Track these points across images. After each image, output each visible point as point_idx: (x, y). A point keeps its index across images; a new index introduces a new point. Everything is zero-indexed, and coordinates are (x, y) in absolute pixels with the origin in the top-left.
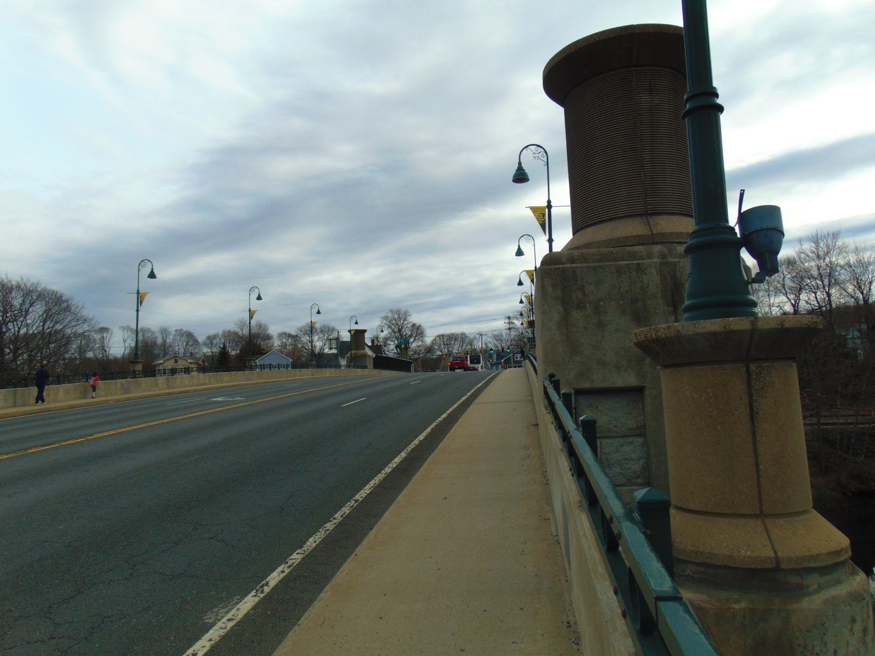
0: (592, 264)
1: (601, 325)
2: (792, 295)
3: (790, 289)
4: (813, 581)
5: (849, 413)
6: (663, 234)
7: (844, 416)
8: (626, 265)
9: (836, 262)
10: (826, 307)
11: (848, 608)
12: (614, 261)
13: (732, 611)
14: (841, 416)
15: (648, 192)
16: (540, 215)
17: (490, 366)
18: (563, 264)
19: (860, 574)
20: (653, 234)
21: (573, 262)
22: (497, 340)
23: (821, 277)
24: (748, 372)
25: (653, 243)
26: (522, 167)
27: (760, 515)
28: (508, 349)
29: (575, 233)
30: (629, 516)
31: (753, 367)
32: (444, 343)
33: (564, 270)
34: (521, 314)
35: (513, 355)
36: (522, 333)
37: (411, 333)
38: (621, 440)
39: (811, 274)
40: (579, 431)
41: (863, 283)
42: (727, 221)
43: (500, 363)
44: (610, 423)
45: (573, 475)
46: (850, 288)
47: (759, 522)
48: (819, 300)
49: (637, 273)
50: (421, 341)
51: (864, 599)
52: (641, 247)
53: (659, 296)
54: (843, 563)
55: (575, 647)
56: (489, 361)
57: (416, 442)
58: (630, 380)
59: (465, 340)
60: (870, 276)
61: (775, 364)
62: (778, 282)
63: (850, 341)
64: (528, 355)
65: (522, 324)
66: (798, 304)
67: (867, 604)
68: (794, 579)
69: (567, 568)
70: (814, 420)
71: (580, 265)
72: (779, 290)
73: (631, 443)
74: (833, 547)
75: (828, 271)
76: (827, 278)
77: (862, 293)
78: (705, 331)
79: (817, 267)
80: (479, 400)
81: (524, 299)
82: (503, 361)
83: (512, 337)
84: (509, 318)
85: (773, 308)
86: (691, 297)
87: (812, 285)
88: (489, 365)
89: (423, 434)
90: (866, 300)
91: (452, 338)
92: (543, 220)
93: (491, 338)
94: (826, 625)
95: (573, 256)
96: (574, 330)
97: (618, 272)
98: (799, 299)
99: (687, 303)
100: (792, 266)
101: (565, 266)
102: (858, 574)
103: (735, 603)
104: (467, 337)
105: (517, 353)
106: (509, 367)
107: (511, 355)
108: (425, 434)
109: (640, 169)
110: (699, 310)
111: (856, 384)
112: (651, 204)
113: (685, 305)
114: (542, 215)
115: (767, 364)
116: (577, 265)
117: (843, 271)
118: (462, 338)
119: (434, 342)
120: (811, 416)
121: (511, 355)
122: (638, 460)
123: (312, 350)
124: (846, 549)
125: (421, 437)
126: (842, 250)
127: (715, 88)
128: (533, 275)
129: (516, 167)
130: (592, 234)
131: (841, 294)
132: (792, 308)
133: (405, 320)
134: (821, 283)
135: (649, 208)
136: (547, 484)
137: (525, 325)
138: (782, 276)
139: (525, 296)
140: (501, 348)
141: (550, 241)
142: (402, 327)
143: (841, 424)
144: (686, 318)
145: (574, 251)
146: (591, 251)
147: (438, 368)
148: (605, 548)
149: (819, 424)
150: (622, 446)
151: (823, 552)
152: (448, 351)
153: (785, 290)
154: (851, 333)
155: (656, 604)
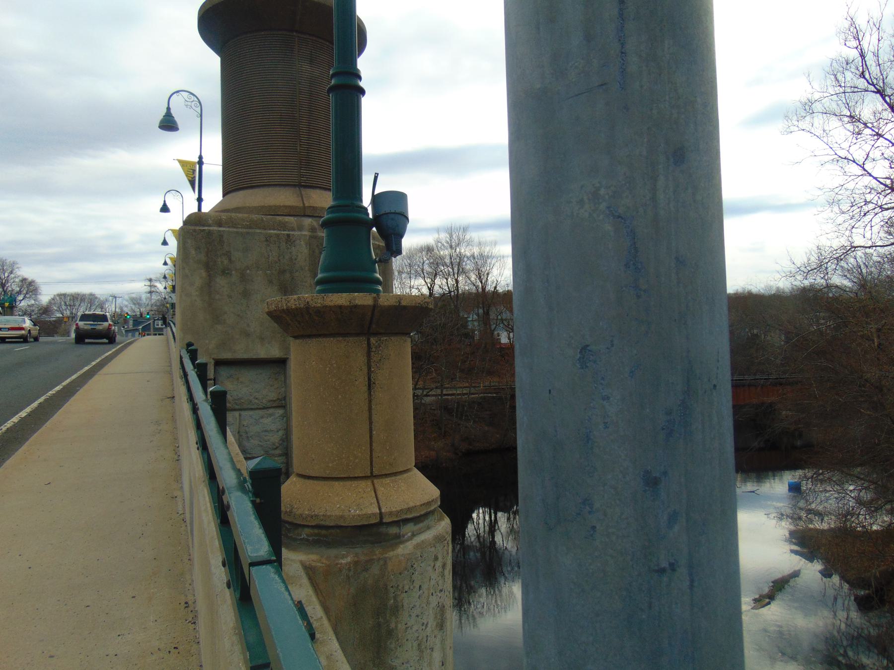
0: (240, 230)
1: (246, 294)
2: (429, 279)
3: (427, 274)
4: (408, 529)
5: (465, 385)
6: (314, 208)
7: (461, 387)
8: (276, 234)
9: (464, 254)
10: (454, 292)
11: (433, 549)
12: (263, 229)
13: (339, 566)
14: (459, 388)
15: (302, 163)
16: (190, 170)
17: (124, 333)
18: (210, 226)
19: (445, 519)
20: (304, 207)
21: (220, 224)
22: (134, 304)
23: (452, 266)
24: (369, 344)
25: (304, 216)
26: (171, 114)
27: (372, 476)
28: (148, 314)
29: (225, 194)
30: (241, 486)
31: (373, 340)
32: (65, 303)
33: (210, 233)
34: (165, 277)
35: (154, 322)
36: (165, 298)
37: (20, 290)
38: (261, 412)
39: (445, 262)
40: (208, 403)
41: (483, 273)
42: (361, 201)
43: (137, 330)
44: (251, 395)
45: (198, 449)
46: (473, 277)
47: (369, 483)
48: (449, 286)
49: (286, 243)
50: (35, 300)
51: (446, 540)
52: (292, 218)
53: (307, 268)
54: (432, 512)
55: (192, 626)
56: (124, 327)
57: (15, 419)
58: (275, 352)
59: (94, 302)
60: (488, 268)
61: (392, 338)
62: (419, 266)
63: (470, 323)
64: (170, 322)
65: (165, 288)
66: (433, 287)
67: (448, 544)
68: (393, 530)
69: (191, 545)
70: (439, 391)
71: (228, 229)
72: (419, 273)
73: (271, 415)
74: (426, 499)
75: (458, 261)
76: (457, 266)
77: (481, 282)
78: (332, 304)
79: (449, 256)
80: (106, 370)
81: (169, 261)
82: (141, 327)
83: (153, 301)
84: (150, 280)
85: (413, 290)
86: (323, 271)
87: (445, 272)
88: (124, 331)
89: (26, 409)
90: (484, 289)
91: (77, 298)
92: (192, 176)
93: (127, 301)
94: (415, 566)
95: (221, 220)
96: (217, 297)
97: (267, 240)
98: (435, 284)
99: (320, 276)
100: (431, 253)
101: (211, 228)
102: (444, 520)
103: (342, 558)
104: (96, 298)
105: (158, 319)
106: (148, 335)
107: (151, 322)
108: (28, 410)
109: (296, 139)
110: (330, 284)
111: (472, 361)
112: (305, 176)
113: (317, 277)
114: (192, 171)
115: (385, 338)
116: (224, 229)
117: (468, 262)
118: (91, 299)
119: (53, 302)
120: (437, 388)
121: (151, 322)
122: (278, 431)
124: (436, 499)
125: (23, 414)
126: (469, 243)
127: (358, 70)
129: (165, 111)
130: (243, 198)
131: (466, 282)
132: (428, 291)
133: (11, 272)
134: (452, 270)
135: (302, 180)
136: (178, 460)
137: (168, 290)
138: (422, 261)
139: (170, 258)
140: (139, 313)
141: (200, 200)
142: (7, 281)
143: (458, 395)
144: (319, 290)
145: (223, 214)
146: (240, 215)
147: (57, 333)
148: (219, 521)
149: (442, 395)
150: (262, 417)
151: (418, 504)
152: (72, 313)
153: (424, 274)
154: (471, 316)
155: (249, 569)
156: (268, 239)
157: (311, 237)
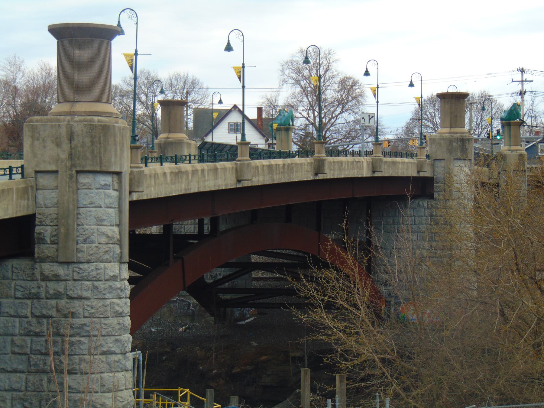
1: (44, 147)
18: (33, 122)
38: (51, 191)
73: (55, 192)
123: (153, 125)
128: (240, 72)
156: (52, 126)
157: (68, 124)
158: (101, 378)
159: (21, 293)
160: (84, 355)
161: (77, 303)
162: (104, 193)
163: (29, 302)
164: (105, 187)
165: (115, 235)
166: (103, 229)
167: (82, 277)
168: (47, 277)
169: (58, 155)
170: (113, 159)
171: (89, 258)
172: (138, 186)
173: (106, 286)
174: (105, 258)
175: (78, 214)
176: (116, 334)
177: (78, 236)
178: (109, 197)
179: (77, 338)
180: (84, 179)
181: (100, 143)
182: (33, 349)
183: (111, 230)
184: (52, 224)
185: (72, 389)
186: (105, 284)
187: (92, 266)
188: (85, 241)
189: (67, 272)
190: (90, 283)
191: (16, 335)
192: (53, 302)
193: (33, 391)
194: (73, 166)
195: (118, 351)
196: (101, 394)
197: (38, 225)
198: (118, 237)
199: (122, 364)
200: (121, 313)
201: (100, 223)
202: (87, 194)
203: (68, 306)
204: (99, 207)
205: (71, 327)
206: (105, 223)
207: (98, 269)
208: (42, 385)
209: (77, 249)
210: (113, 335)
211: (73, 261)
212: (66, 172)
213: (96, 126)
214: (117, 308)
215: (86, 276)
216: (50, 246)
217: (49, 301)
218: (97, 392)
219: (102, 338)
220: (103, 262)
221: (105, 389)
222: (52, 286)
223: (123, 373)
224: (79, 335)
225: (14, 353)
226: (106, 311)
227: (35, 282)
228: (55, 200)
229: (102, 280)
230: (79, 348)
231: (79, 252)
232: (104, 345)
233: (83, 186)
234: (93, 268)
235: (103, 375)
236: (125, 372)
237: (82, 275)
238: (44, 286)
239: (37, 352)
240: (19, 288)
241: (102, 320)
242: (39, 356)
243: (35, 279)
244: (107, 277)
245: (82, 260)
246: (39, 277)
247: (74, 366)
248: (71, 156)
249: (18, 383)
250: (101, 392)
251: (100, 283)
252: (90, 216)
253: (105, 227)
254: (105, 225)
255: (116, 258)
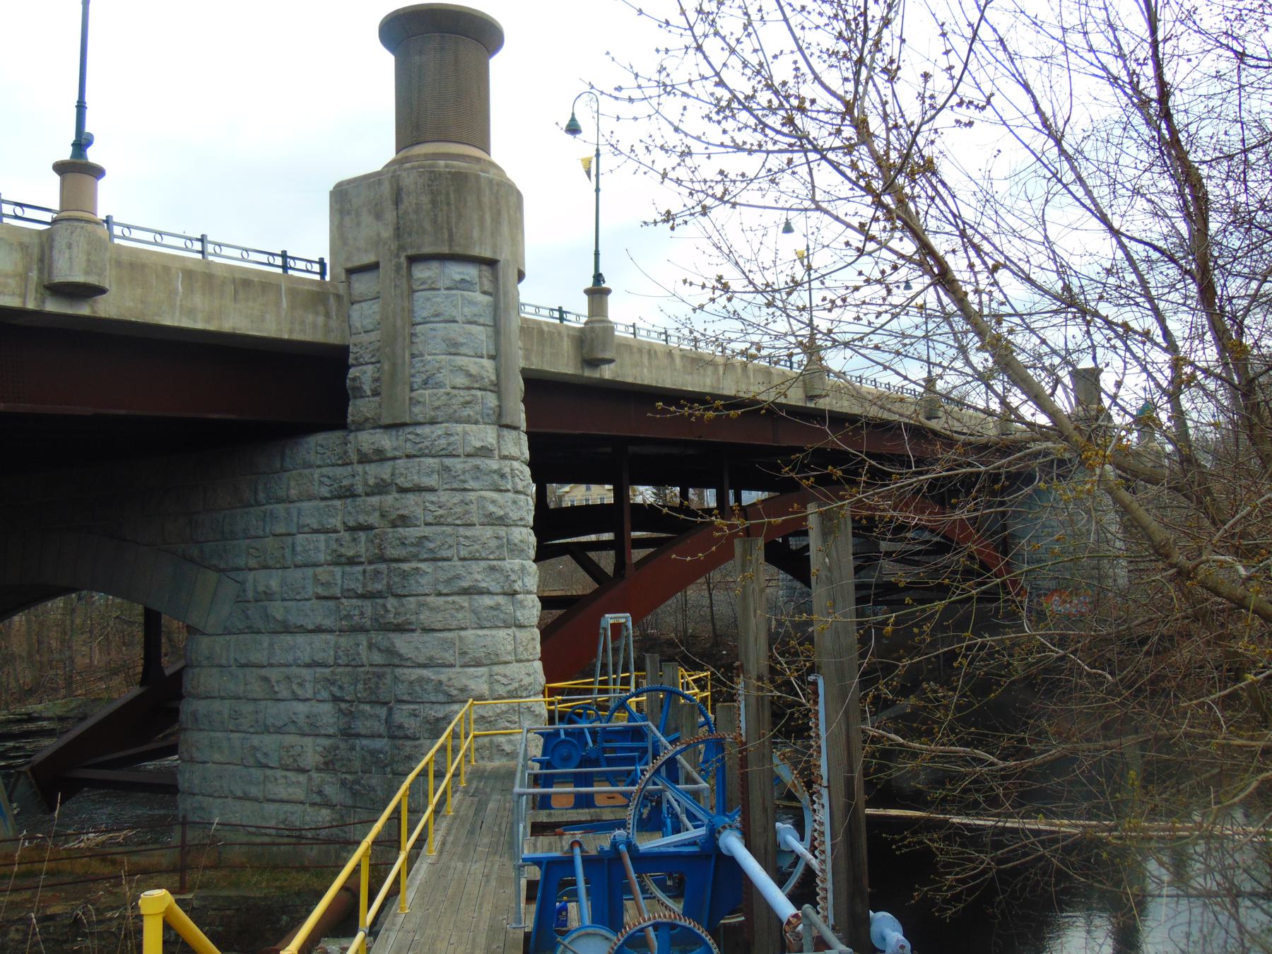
1: (358, 224)
158: (461, 638)
159: (328, 489)
160: (426, 595)
161: (411, 498)
162: (462, 296)
163: (338, 503)
164: (464, 284)
165: (485, 374)
166: (460, 361)
167: (420, 449)
168: (366, 455)
169: (378, 235)
170: (476, 234)
171: (433, 414)
172: (604, 350)
173: (468, 466)
174: (465, 413)
175: (413, 335)
176: (491, 557)
177: (413, 376)
178: (472, 303)
179: (414, 565)
180: (422, 272)
181: (449, 204)
182: (345, 587)
183: (476, 363)
184: (373, 360)
185: (406, 659)
186: (465, 462)
187: (439, 430)
188: (425, 382)
189: (395, 444)
190: (436, 460)
191: (321, 565)
192: (374, 500)
193: (347, 665)
194: (401, 248)
195: (494, 587)
196: (459, 670)
197: (354, 366)
198: (493, 378)
199: (506, 613)
200: (501, 518)
201: (453, 350)
202: (429, 299)
203: (397, 505)
204: (451, 322)
205: (403, 544)
206: (463, 350)
207: (451, 435)
208: (358, 654)
209: (411, 399)
210: (483, 559)
211: (403, 420)
212: (391, 260)
213: (440, 174)
214: (492, 508)
215: (427, 447)
216: (371, 399)
217: (368, 499)
218: (452, 666)
219: (460, 563)
220: (461, 423)
221: (467, 659)
222: (374, 472)
223: (510, 631)
224: (416, 557)
225: (319, 598)
226: (467, 512)
227: (349, 468)
228: (378, 317)
229: (459, 456)
230: (417, 582)
231: (415, 405)
232: (465, 577)
233: (422, 284)
234: (440, 432)
235: (463, 633)
236: (514, 629)
237: (420, 446)
238: (361, 473)
239: (351, 594)
240: (325, 480)
241: (461, 529)
242: (354, 601)
243: (348, 461)
244: (469, 450)
245: (420, 418)
246: (354, 458)
247: (408, 616)
248: (398, 232)
249: (324, 651)
250: (461, 666)
251: (457, 460)
252: (435, 337)
253: (464, 358)
254: (464, 355)
255: (488, 415)
